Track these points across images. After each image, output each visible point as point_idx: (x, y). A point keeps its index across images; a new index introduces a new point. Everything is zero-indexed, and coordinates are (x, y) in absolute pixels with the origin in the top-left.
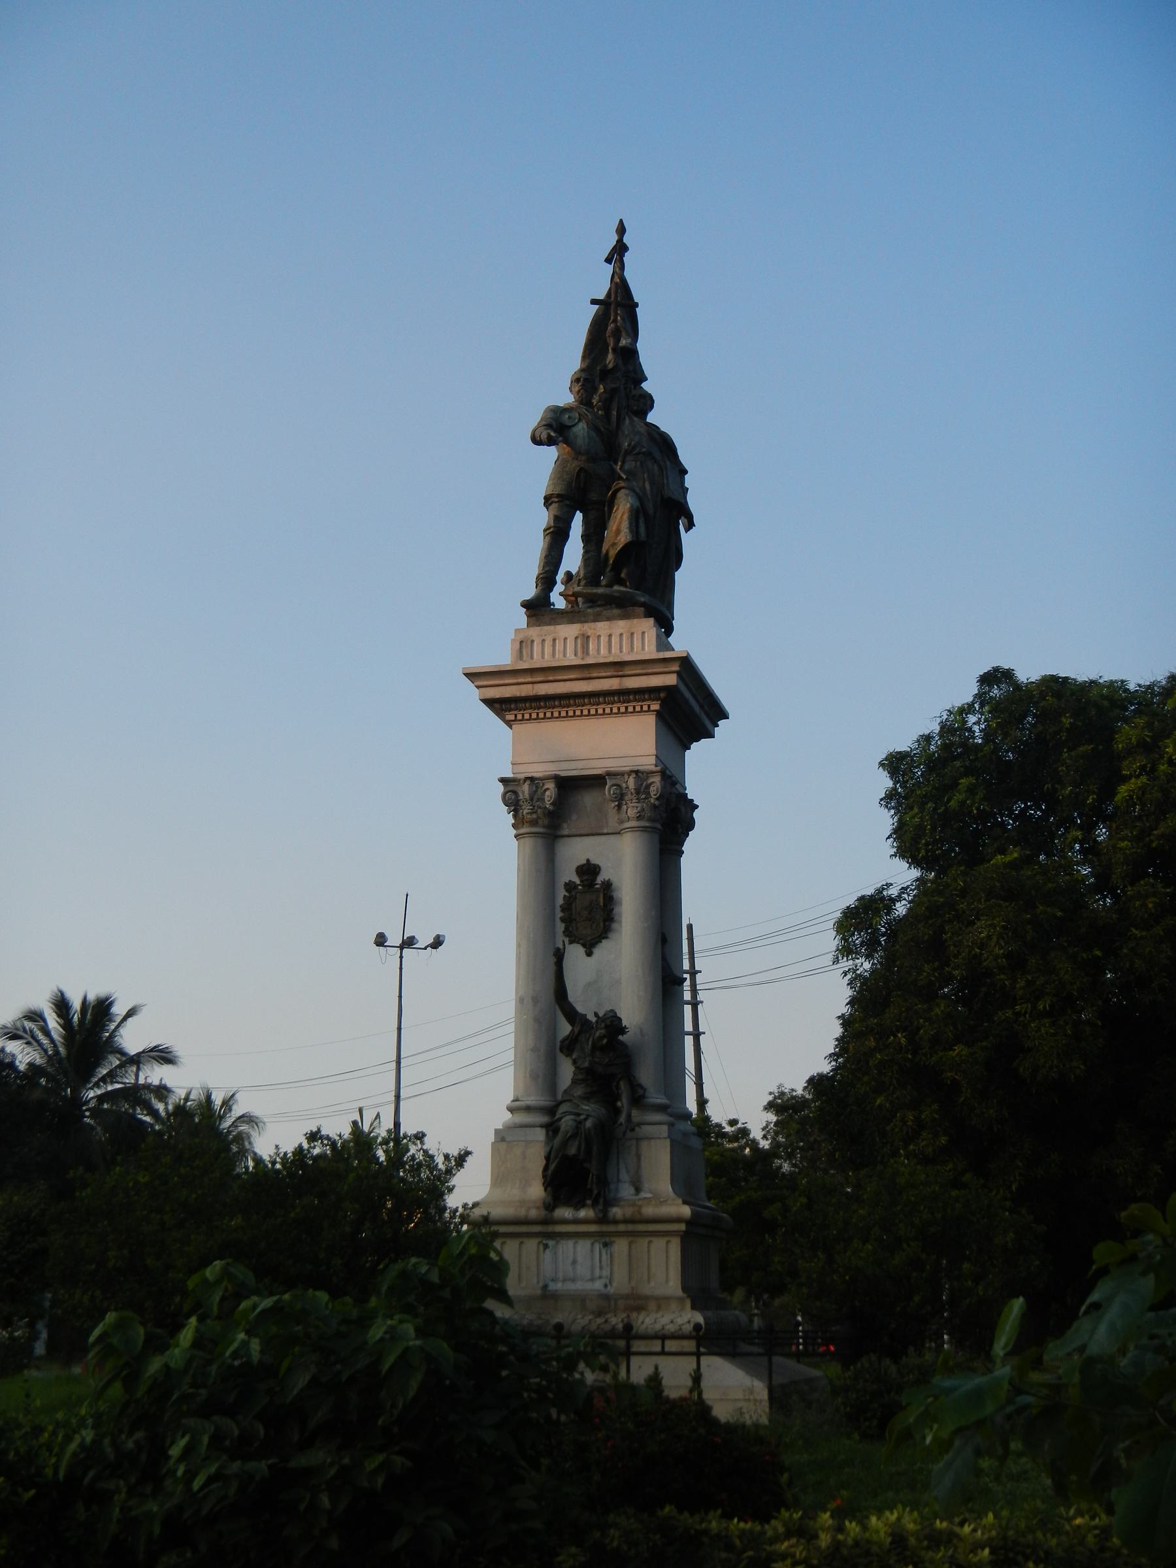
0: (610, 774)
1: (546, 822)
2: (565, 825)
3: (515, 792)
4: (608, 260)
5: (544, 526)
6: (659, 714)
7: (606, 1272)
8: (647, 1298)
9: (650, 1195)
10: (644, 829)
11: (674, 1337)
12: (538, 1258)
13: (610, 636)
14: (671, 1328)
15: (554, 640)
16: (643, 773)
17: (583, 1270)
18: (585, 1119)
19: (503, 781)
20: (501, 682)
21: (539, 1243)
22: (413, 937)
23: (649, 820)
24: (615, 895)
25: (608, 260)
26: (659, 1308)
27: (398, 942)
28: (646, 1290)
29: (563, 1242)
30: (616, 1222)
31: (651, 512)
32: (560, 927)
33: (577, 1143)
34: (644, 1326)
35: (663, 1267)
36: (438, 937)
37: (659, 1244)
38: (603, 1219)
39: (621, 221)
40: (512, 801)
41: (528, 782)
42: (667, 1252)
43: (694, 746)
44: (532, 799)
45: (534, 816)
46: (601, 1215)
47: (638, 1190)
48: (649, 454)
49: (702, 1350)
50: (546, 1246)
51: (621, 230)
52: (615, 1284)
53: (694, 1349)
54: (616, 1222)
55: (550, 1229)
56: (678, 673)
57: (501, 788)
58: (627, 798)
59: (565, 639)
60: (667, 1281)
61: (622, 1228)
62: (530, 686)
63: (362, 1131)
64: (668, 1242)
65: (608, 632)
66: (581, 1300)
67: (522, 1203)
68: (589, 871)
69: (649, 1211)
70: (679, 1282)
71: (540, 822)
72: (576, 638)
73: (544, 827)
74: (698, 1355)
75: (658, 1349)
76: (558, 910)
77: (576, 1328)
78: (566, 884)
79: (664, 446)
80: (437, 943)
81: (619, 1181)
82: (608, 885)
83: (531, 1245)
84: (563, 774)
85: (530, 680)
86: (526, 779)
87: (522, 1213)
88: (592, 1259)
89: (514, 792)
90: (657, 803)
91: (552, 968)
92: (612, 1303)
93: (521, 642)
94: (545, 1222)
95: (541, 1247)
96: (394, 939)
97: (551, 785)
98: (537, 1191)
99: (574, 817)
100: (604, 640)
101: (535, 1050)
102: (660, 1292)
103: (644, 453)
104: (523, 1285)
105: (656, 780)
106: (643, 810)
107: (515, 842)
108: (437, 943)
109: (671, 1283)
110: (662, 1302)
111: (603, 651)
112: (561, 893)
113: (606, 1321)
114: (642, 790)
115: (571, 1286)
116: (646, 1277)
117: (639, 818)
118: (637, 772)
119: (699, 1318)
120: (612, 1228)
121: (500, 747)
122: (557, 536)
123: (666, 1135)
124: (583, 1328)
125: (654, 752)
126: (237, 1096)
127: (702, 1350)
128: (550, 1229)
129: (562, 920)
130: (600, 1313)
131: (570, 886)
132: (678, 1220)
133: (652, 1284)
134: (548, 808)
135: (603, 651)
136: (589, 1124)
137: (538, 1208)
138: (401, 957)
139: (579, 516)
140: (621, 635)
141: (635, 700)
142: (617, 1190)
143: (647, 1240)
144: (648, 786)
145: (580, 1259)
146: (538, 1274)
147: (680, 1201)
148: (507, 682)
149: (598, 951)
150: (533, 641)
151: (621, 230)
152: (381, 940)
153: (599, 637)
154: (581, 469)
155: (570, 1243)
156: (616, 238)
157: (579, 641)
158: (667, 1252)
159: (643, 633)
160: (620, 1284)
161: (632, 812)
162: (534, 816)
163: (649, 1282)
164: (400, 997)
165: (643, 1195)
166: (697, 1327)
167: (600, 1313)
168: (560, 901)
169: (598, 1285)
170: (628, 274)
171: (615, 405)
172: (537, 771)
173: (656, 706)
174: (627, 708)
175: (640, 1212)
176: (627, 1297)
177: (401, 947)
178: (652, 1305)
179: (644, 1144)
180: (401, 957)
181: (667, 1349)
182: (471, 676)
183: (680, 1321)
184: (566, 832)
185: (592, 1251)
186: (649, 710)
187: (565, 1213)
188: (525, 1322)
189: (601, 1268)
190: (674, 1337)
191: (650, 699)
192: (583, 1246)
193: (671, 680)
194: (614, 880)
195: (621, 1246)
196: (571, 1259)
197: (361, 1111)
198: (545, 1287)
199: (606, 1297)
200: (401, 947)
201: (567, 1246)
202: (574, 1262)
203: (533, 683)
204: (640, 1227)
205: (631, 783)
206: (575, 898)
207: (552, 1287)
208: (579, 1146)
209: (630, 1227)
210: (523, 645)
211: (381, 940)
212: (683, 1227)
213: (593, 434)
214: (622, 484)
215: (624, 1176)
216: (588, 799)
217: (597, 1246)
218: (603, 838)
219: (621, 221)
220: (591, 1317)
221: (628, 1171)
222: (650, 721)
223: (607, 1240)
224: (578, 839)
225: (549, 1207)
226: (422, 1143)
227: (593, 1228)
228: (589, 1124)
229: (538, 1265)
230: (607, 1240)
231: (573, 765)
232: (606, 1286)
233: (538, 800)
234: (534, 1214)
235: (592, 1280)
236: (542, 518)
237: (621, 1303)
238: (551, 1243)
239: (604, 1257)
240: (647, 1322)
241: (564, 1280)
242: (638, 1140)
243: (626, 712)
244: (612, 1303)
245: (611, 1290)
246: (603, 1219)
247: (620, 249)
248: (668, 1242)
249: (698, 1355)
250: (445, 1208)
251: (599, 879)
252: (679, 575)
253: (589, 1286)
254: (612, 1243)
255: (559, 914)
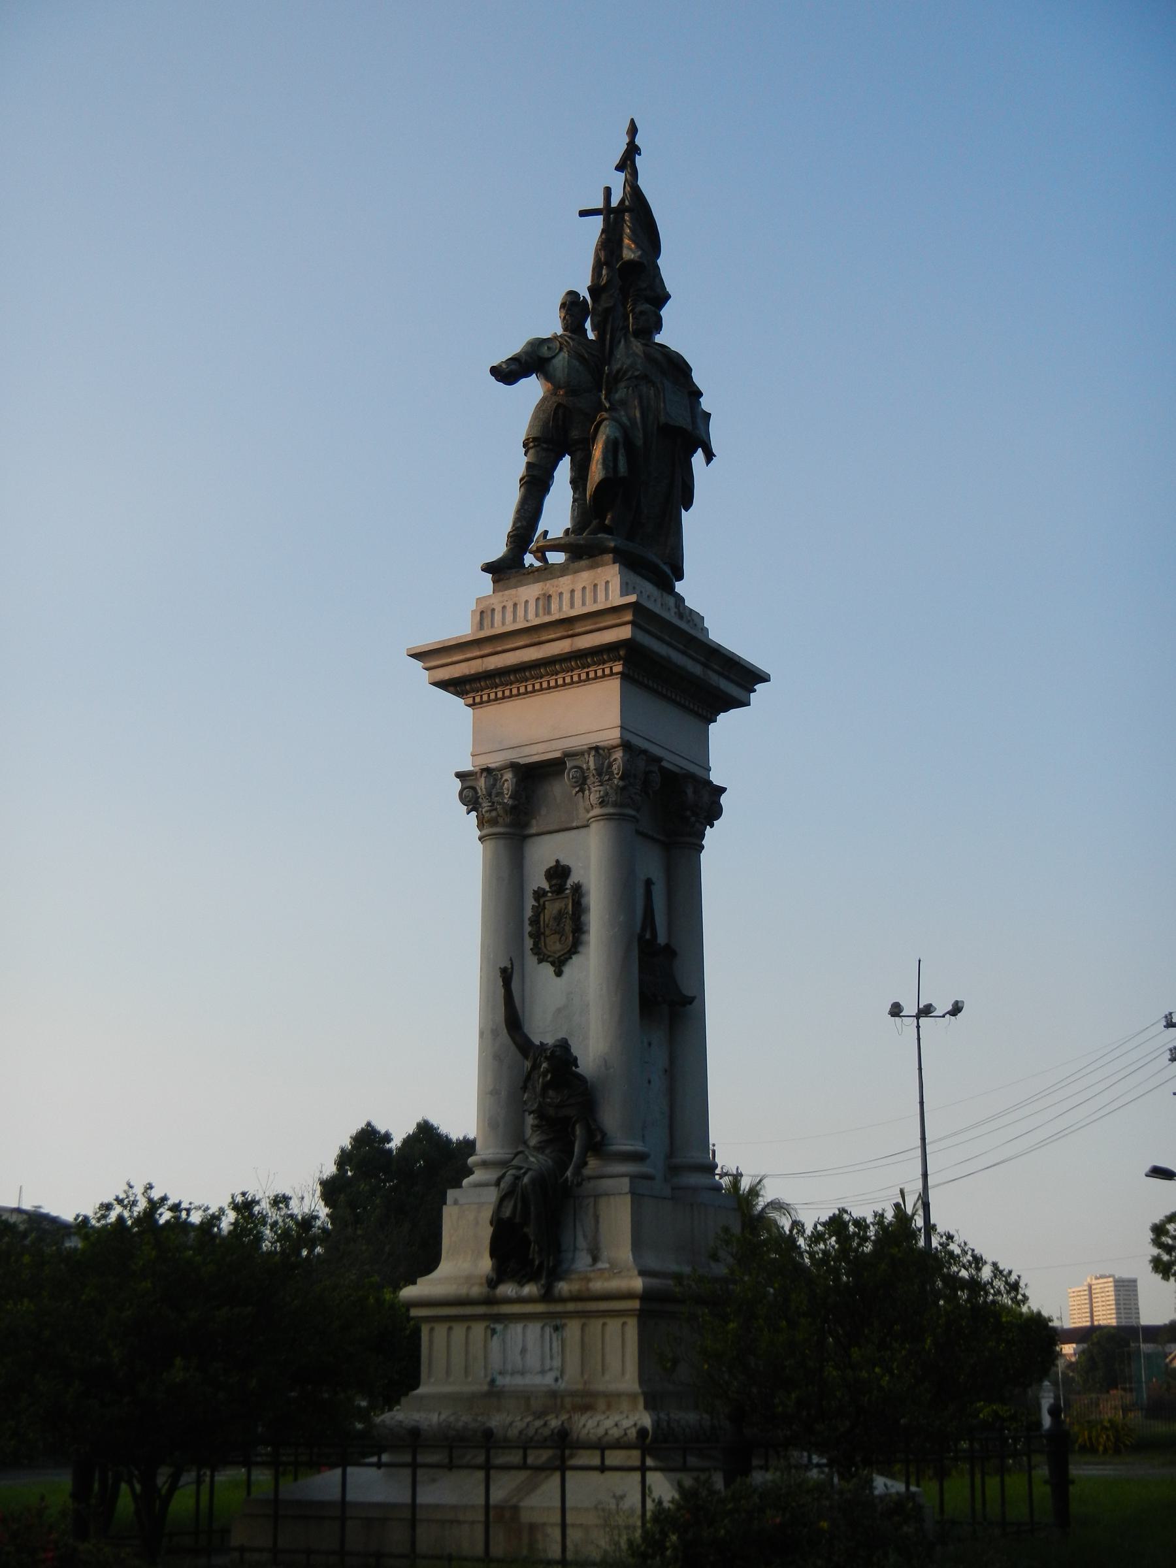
0: (568, 755)
1: (508, 820)
2: (534, 822)
3: (473, 788)
4: (620, 168)
5: (520, 476)
6: (624, 676)
7: (557, 1363)
8: (595, 1395)
9: (607, 1266)
10: (608, 817)
11: (618, 1445)
12: (485, 1347)
13: (573, 591)
14: (616, 1433)
15: (515, 605)
16: (603, 749)
17: (533, 1361)
18: (525, 1173)
19: (459, 775)
20: (449, 660)
21: (487, 1327)
22: (931, 1005)
23: (615, 805)
24: (584, 901)
25: (620, 168)
26: (609, 1407)
27: (914, 1012)
28: (600, 1386)
29: (512, 1326)
30: (562, 1300)
31: (639, 442)
32: (529, 943)
33: (512, 1203)
34: (585, 1431)
35: (616, 1358)
36: (957, 1003)
37: (614, 1325)
38: (548, 1296)
39: (632, 120)
40: (470, 799)
41: (485, 774)
42: (623, 1334)
43: (722, 717)
44: (490, 795)
45: (494, 814)
46: (543, 1292)
47: (595, 1259)
48: (645, 378)
49: (649, 1462)
50: (494, 1331)
51: (633, 130)
52: (566, 1377)
53: (638, 1463)
54: (562, 1300)
55: (495, 1310)
56: (633, 623)
57: (457, 784)
58: (589, 782)
59: (527, 602)
60: (623, 1373)
61: (571, 1307)
62: (479, 661)
63: (905, 1213)
64: (624, 1324)
65: (571, 587)
66: (525, 1396)
67: (468, 1279)
68: (558, 873)
69: (598, 1286)
70: (636, 1375)
71: (500, 820)
72: (538, 599)
73: (506, 826)
74: (643, 1469)
75: (596, 1461)
76: (527, 922)
77: (513, 1433)
78: (535, 892)
79: (676, 369)
80: (956, 1010)
81: (575, 1249)
82: (577, 889)
83: (479, 1329)
84: (522, 761)
85: (478, 653)
86: (483, 770)
87: (463, 1291)
88: (542, 1347)
89: (475, 790)
90: (621, 783)
91: (501, 991)
92: (559, 1401)
93: (482, 612)
94: (489, 1301)
95: (489, 1332)
96: (910, 1009)
97: (508, 775)
98: (486, 1265)
99: (543, 812)
100: (566, 597)
101: (494, 1092)
102: (613, 1387)
103: (636, 377)
104: (470, 1379)
105: (618, 755)
106: (607, 794)
107: (480, 846)
108: (956, 1010)
109: (628, 1376)
110: (612, 1399)
111: (566, 607)
112: (530, 902)
113: (545, 1424)
114: (603, 771)
115: (519, 1381)
116: (599, 1368)
117: (602, 803)
118: (597, 749)
119: (647, 1421)
120: (559, 1308)
121: (453, 737)
122: (536, 486)
123: (626, 1189)
124: (521, 1432)
125: (618, 723)
126: (764, 1181)
127: (649, 1462)
128: (495, 1310)
129: (531, 935)
130: (539, 1415)
131: (539, 894)
132: (629, 1296)
133: (607, 1377)
134: (509, 801)
135: (566, 607)
136: (526, 1180)
137: (481, 1284)
138: (918, 1027)
139: (567, 459)
140: (584, 588)
141: (594, 664)
142: (573, 1260)
143: (601, 1321)
144: (610, 765)
145: (530, 1346)
146: (485, 1368)
147: (636, 1272)
148: (455, 659)
149: (567, 970)
150: (493, 610)
151: (633, 130)
152: (896, 1010)
153: (561, 594)
154: (559, 405)
155: (519, 1327)
156: (627, 140)
157: (541, 602)
158: (623, 1334)
159: (607, 583)
160: (572, 1380)
161: (594, 798)
162: (494, 814)
163: (603, 1374)
164: (920, 1069)
165: (600, 1265)
166: (643, 1432)
167: (539, 1415)
168: (529, 913)
169: (549, 1379)
170: (642, 183)
171: (609, 327)
172: (494, 761)
173: (618, 668)
174: (588, 673)
175: (588, 1289)
176: (573, 1394)
177: (918, 1017)
178: (601, 1404)
179: (603, 1202)
180: (918, 1027)
181: (608, 1462)
182: (417, 656)
183: (626, 1423)
184: (533, 831)
185: (542, 1336)
186: (612, 674)
187: (507, 1289)
188: (460, 1424)
189: (552, 1358)
190: (618, 1445)
191: (610, 660)
192: (534, 1329)
193: (625, 633)
194: (583, 881)
195: (573, 1329)
196: (520, 1346)
197: (902, 1192)
198: (493, 1381)
199: (553, 1394)
200: (918, 1017)
201: (517, 1329)
202: (524, 1351)
203: (482, 657)
204: (592, 1307)
205: (591, 762)
206: (544, 908)
207: (503, 1381)
208: (515, 1207)
209: (580, 1306)
210: (484, 615)
211: (896, 1010)
212: (636, 1304)
213: (576, 363)
214: (605, 415)
215: (582, 1243)
216: (560, 789)
217: (548, 1330)
218: (573, 833)
219: (632, 120)
220: (529, 1419)
221: (585, 1236)
222: (614, 685)
223: (558, 1322)
224: (547, 837)
225: (492, 1283)
226: (287, 1206)
227: (540, 1308)
228: (526, 1180)
229: (486, 1358)
230: (558, 1322)
231: (540, 748)
232: (556, 1380)
233: (498, 794)
234: (476, 1291)
235: (543, 1372)
236: (518, 463)
237: (568, 1400)
238: (499, 1327)
239: (555, 1344)
240: (590, 1425)
241: (513, 1374)
242: (597, 1196)
243: (588, 679)
244: (559, 1401)
245: (562, 1385)
246: (548, 1296)
247: (632, 150)
248: (624, 1324)
249: (643, 1469)
250: (543, 1286)
251: (570, 882)
252: (688, 518)
253: (538, 1380)
254: (563, 1326)
255: (528, 928)
